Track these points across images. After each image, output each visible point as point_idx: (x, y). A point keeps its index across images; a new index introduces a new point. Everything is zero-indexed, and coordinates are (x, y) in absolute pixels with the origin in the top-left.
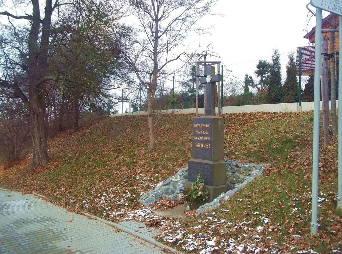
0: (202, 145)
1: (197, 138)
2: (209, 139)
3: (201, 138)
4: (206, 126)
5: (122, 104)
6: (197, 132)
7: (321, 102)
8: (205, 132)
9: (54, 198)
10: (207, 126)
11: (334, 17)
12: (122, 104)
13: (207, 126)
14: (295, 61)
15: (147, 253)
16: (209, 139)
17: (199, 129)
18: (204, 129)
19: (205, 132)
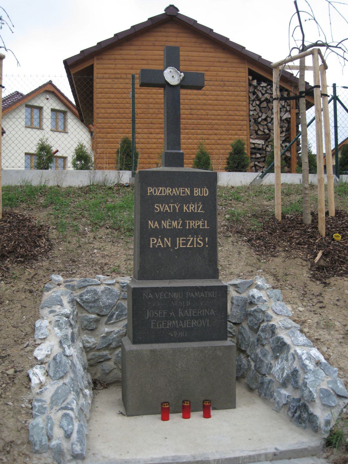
0: (180, 241)
1: (160, 224)
2: (203, 226)
3: (175, 224)
4: (192, 192)
5: (303, 40)
6: (159, 208)
7: (324, 152)
8: (192, 208)
9: (84, 68)
10: (197, 192)
11: (2, 135)
12: (303, 40)
13: (197, 192)
14: (111, 346)
15: (46, 462)
16: (203, 226)
17: (166, 200)
18: (164, 216)
19: (192, 208)
